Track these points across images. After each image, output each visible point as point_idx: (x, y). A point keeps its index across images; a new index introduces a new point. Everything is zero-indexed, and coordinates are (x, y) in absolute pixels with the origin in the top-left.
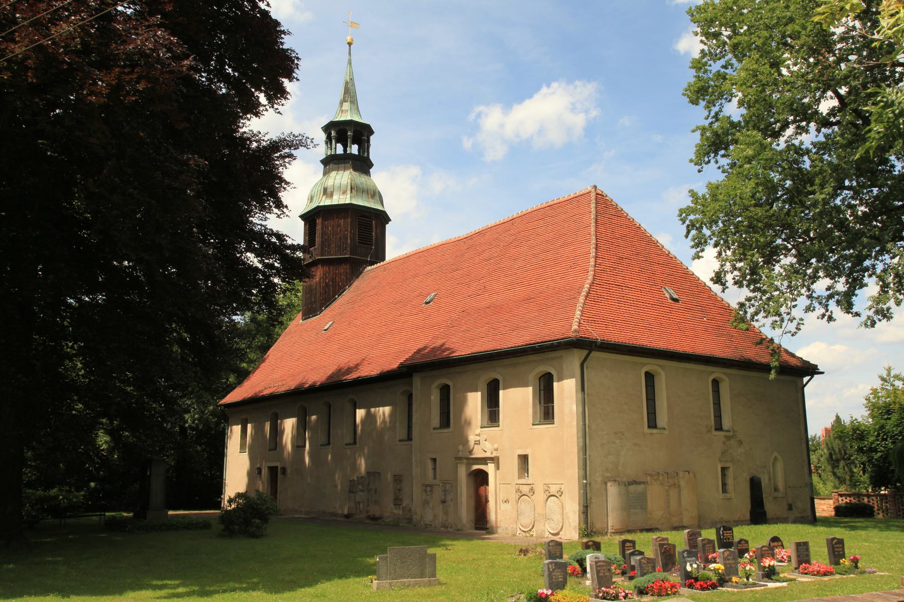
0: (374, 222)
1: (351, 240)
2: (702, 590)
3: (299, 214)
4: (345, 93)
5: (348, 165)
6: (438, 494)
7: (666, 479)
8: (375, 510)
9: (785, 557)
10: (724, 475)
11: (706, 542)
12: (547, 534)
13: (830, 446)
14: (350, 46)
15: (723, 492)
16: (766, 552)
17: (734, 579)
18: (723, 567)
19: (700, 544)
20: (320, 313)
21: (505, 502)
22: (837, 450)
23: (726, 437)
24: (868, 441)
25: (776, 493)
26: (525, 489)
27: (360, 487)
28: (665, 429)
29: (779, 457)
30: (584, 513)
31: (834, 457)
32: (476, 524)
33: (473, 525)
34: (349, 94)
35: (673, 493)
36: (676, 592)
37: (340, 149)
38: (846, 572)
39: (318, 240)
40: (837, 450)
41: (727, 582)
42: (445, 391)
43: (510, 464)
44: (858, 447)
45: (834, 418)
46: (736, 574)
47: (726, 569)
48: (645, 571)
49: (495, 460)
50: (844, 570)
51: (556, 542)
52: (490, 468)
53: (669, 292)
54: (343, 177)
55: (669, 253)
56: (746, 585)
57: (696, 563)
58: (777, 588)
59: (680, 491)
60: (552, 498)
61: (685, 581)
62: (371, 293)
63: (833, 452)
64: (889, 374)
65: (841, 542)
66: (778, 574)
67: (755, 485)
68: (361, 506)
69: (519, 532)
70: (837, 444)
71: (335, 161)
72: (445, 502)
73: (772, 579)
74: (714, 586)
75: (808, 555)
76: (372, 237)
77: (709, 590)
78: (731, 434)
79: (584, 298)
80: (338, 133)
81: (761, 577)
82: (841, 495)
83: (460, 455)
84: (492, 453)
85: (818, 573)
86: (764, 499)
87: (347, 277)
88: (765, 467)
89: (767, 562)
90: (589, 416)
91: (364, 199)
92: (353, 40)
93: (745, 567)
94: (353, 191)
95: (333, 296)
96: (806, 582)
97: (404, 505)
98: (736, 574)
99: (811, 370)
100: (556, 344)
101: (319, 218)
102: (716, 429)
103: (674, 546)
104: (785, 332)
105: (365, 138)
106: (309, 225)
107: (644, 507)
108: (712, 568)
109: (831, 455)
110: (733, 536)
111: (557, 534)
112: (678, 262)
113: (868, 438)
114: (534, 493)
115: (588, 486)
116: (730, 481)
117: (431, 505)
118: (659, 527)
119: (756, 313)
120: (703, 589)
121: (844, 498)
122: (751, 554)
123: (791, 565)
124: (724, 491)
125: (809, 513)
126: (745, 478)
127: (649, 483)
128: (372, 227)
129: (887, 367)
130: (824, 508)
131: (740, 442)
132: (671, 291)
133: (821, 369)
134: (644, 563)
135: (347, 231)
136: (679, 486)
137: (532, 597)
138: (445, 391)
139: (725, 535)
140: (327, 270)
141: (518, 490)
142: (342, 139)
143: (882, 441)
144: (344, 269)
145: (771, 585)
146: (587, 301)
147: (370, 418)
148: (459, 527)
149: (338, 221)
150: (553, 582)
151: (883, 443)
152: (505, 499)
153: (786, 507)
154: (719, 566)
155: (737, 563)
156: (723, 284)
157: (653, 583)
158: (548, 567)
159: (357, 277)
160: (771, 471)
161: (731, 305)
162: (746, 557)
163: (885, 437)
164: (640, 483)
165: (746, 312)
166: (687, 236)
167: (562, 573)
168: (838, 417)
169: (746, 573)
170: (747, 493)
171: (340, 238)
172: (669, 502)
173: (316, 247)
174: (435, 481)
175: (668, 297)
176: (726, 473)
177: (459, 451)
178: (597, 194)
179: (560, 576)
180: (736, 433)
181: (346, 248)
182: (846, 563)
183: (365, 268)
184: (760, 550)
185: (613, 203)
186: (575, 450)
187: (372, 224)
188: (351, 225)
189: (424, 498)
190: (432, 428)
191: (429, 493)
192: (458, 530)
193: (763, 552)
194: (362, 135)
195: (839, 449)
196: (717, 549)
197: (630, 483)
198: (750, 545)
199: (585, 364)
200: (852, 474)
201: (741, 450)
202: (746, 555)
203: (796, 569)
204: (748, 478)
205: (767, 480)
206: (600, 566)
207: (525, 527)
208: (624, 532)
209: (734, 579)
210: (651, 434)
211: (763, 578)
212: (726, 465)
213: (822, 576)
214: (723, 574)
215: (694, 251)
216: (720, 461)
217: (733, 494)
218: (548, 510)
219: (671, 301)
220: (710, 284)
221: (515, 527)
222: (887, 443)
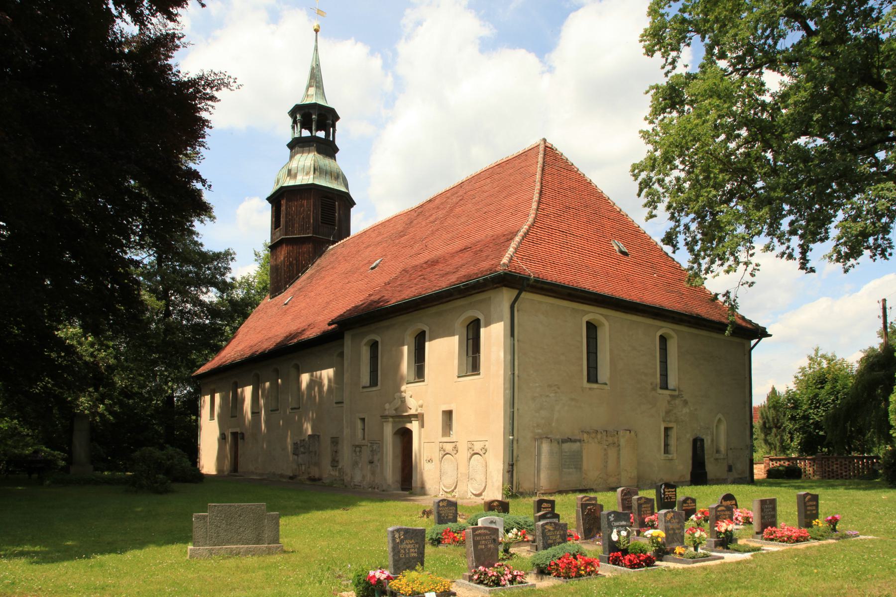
0: (337, 203)
1: (313, 220)
2: (631, 568)
3: (266, 197)
4: (311, 79)
5: (313, 148)
6: (366, 454)
7: (605, 437)
8: (315, 472)
9: (740, 518)
10: (667, 436)
11: (642, 501)
12: (470, 494)
13: (765, 415)
14: (316, 33)
15: (665, 453)
16: (722, 513)
17: (678, 549)
18: (663, 535)
19: (635, 504)
20: (285, 291)
21: (429, 461)
22: (771, 419)
23: (671, 396)
24: (801, 409)
25: (717, 455)
26: (449, 447)
27: (302, 449)
28: (606, 384)
29: (723, 419)
30: (508, 472)
31: (767, 426)
32: (402, 485)
33: (399, 485)
34: (315, 79)
35: (612, 453)
36: (592, 571)
37: (306, 133)
38: (822, 536)
39: (283, 220)
40: (771, 419)
41: (668, 553)
42: (374, 346)
43: (434, 421)
44: (792, 415)
45: (771, 390)
46: (681, 542)
47: (667, 537)
48: (550, 541)
49: (419, 417)
50: (820, 533)
51: (449, 501)
52: (414, 426)
53: (617, 245)
54: (307, 159)
55: (621, 210)
56: (694, 558)
57: (626, 530)
58: (739, 563)
59: (619, 450)
60: (476, 456)
61: (609, 554)
62: (329, 267)
63: (767, 421)
64: (816, 355)
65: (773, 502)
66: (736, 540)
67: (698, 445)
68: (303, 468)
69: (441, 493)
70: (771, 413)
71: (300, 145)
72: (373, 462)
73: (728, 548)
74: (649, 562)
75: (774, 516)
76: (335, 218)
77: (642, 566)
78: (676, 393)
79: (521, 238)
80: (303, 116)
81: (713, 545)
82: (772, 460)
83: (387, 413)
84: (417, 410)
85: (788, 540)
86: (706, 460)
87: (309, 256)
88: (708, 428)
89: (723, 526)
90: (518, 365)
91: (327, 180)
92: (319, 27)
93: (694, 533)
94: (316, 172)
95: (297, 274)
96: (778, 552)
97: (340, 467)
98: (681, 542)
99: (760, 333)
100: (481, 281)
101: (283, 199)
102: (661, 388)
103: (601, 507)
104: (741, 283)
105: (330, 122)
106: (276, 207)
107: (579, 467)
108: (649, 536)
109: (764, 423)
110: (676, 495)
111: (479, 495)
112: (629, 220)
113: (802, 406)
114: (457, 451)
115: (515, 443)
116: (673, 442)
117: (360, 465)
118: (594, 487)
119: (713, 262)
120: (633, 566)
121: (774, 462)
122: (699, 515)
123: (752, 529)
124: (666, 451)
125: (747, 474)
126: (689, 437)
127: (586, 441)
128: (335, 208)
129: (815, 348)
130: (759, 471)
131: (686, 403)
132: (621, 245)
133: (769, 331)
134: (550, 530)
135: (310, 211)
136: (619, 445)
137: (362, 581)
138: (374, 346)
139: (666, 493)
140: (291, 249)
141: (442, 449)
142: (306, 125)
143: (815, 409)
144: (307, 248)
145: (730, 557)
146: (524, 241)
147: (315, 383)
148: (384, 488)
149: (301, 202)
150: (401, 559)
151: (815, 410)
152: (429, 459)
153: (726, 468)
154: (659, 533)
155: (682, 528)
156: (674, 246)
157: (560, 559)
158: (394, 537)
159: (320, 256)
160: (715, 433)
161: (682, 265)
162: (692, 520)
163: (818, 405)
164: (575, 441)
165: (700, 265)
166: (639, 195)
167: (417, 546)
168: (773, 389)
169: (695, 542)
170: (689, 454)
171: (303, 218)
172: (607, 462)
173: (281, 227)
174: (364, 441)
175: (617, 250)
176: (669, 433)
177: (385, 410)
178: (546, 147)
179: (413, 550)
180: (682, 393)
181: (309, 227)
182: (820, 525)
183: (328, 247)
184: (714, 511)
185: (563, 157)
186: (502, 402)
187: (335, 205)
188: (313, 206)
189: (354, 458)
190: (361, 387)
191: (358, 453)
192: (383, 491)
193: (718, 513)
194: (327, 119)
195: (773, 417)
196: (656, 511)
197: (564, 441)
198: (698, 505)
199: (516, 305)
200: (782, 441)
201: (686, 410)
202: (693, 517)
203: (757, 533)
204: (691, 439)
205: (709, 441)
206: (480, 535)
207: (448, 488)
208: (555, 493)
209: (678, 549)
210: (590, 389)
211: (716, 546)
212: (670, 425)
213: (794, 543)
214: (664, 544)
215: (647, 210)
216: (664, 421)
217: (675, 455)
218: (471, 469)
219: (620, 254)
220: (661, 244)
221: (438, 487)
222: (819, 410)
